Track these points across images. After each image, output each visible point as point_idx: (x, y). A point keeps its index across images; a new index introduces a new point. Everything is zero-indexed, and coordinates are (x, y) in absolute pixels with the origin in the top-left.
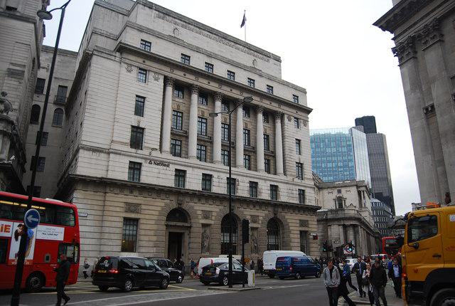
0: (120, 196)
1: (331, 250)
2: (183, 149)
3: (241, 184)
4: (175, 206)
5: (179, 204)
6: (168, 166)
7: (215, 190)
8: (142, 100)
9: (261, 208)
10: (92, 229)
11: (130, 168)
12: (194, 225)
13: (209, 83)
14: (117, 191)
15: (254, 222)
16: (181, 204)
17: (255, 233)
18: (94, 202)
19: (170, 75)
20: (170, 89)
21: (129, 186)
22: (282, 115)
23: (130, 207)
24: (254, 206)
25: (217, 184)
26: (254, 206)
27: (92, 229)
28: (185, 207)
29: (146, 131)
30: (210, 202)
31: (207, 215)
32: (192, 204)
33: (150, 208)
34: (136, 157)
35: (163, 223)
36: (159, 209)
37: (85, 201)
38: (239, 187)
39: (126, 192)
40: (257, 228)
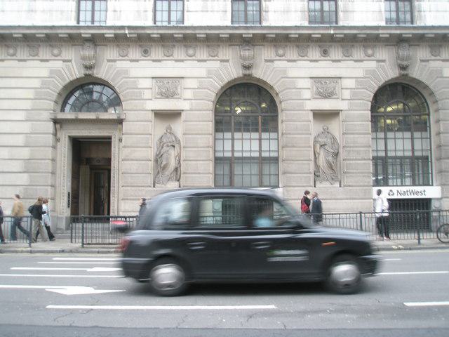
0: (300, 63)
1: (377, 179)
4: (391, 73)
5: (87, 67)
9: (347, 55)
12: (130, 116)
14: (23, 53)
21: (16, 39)
24: (325, 53)
26: (325, 53)
28: (416, 72)
31: (325, 88)
32: (435, 65)
33: (13, 82)
35: (47, 115)
36: (36, 83)
39: (314, 53)
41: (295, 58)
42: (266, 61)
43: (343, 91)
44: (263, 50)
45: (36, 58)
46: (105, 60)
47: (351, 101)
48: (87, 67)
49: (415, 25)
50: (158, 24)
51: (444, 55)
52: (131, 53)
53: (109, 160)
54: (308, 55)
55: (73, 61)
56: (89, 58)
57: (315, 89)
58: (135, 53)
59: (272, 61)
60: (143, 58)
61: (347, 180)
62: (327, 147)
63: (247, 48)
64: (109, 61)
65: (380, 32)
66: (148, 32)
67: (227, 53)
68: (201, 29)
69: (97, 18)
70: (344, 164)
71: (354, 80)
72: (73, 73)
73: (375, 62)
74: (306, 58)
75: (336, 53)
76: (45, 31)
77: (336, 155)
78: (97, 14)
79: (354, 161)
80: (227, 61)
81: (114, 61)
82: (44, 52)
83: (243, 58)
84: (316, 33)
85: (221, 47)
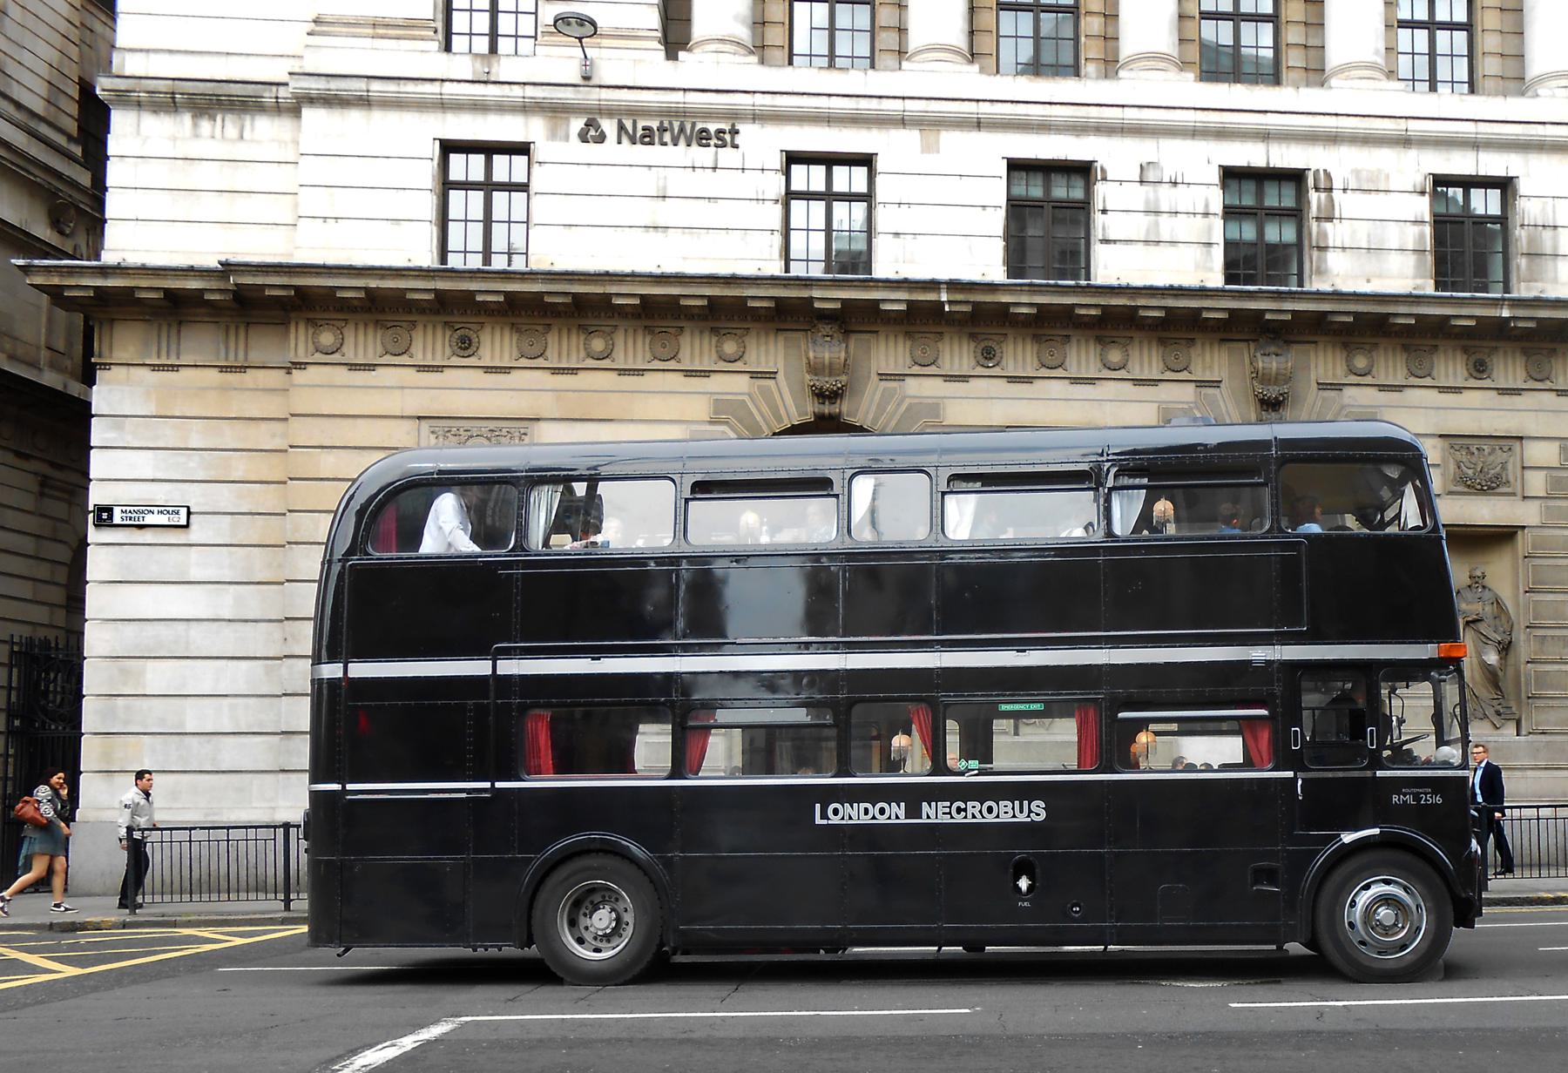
2: (1293, 35)
3: (1345, 203)
5: (821, 395)
6: (728, 139)
9: (466, 346)
10: (225, 603)
14: (362, 344)
15: (1486, 485)
16: (834, 396)
17: (1500, 572)
18: (229, 435)
21: (622, 312)
24: (466, 346)
25: (1137, 226)
26: (1480, 369)
27: (225, 603)
34: (479, 107)
37: (168, 433)
38: (1335, 233)
39: (1451, 368)
40: (1500, 537)
41: (1399, 380)
42: (1323, 386)
43: (1528, 474)
44: (1312, 354)
45: (672, 365)
46: (875, 377)
47: (1551, 503)
48: (821, 395)
49: (1514, 295)
50: (454, 261)
51: (1011, 363)
52: (947, 357)
53: (519, 675)
54: (1435, 373)
55: (780, 376)
56: (831, 370)
57: (1452, 467)
58: (958, 355)
59: (1338, 387)
60: (980, 371)
61: (1534, 718)
62: (1482, 627)
63: (1273, 349)
64: (884, 377)
65: (816, 293)
66: (1006, 298)
68: (1153, 296)
69: (498, 243)
70: (1528, 676)
71: (1557, 444)
72: (782, 412)
73: (746, 377)
74: (1428, 381)
75: (1508, 371)
76: (708, 291)
77: (1505, 649)
78: (498, 231)
79: (1556, 667)
80: (1216, 384)
81: (901, 377)
82: (695, 349)
83: (1260, 377)
84: (1024, 302)
85: (1199, 345)
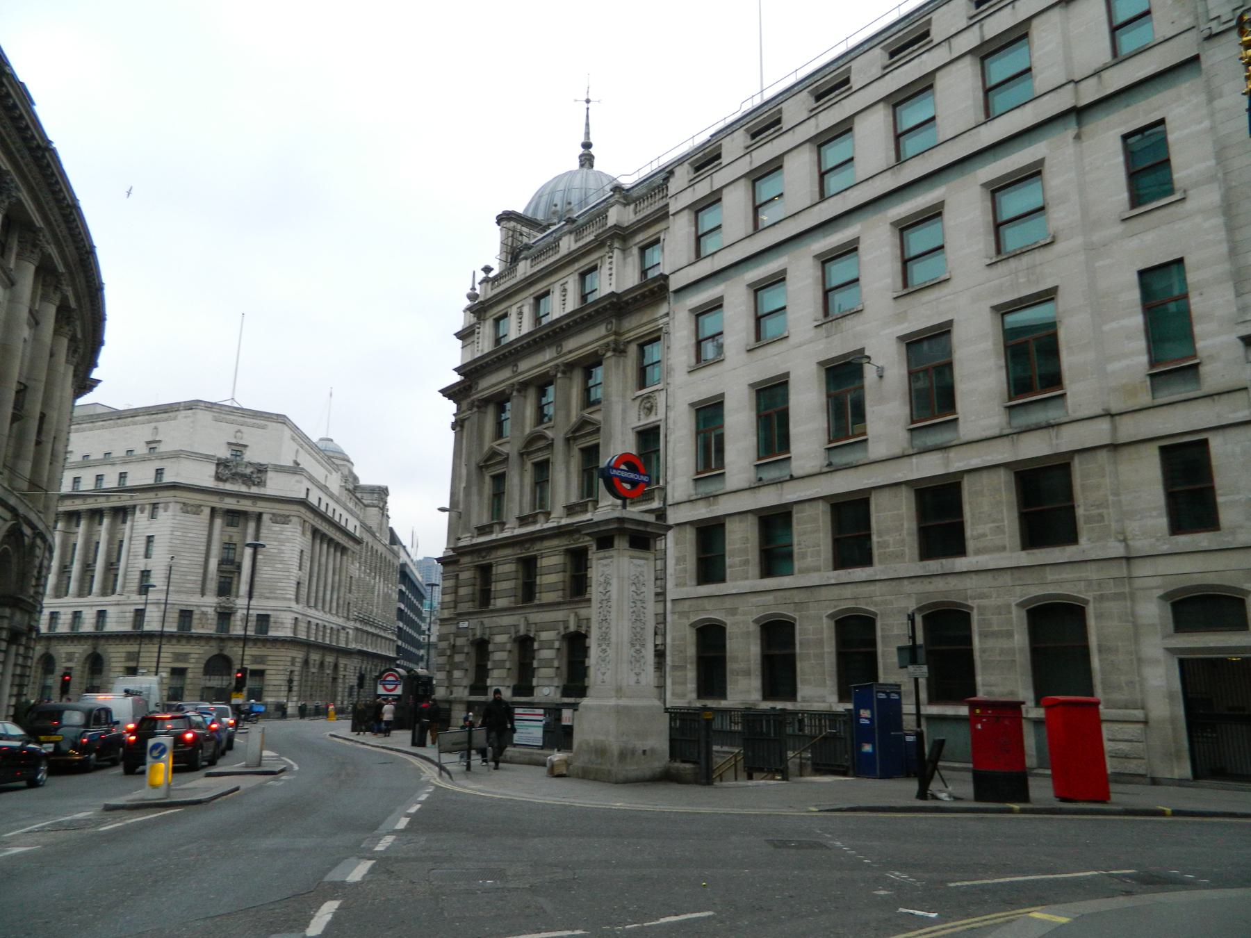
4: (215, 652)
7: (196, 630)
8: (233, 547)
11: (180, 616)
13: (156, 495)
19: (218, 505)
20: (218, 522)
22: (259, 516)
23: (178, 657)
29: (152, 572)
30: (76, 642)
31: (70, 657)
67: (213, 643)
